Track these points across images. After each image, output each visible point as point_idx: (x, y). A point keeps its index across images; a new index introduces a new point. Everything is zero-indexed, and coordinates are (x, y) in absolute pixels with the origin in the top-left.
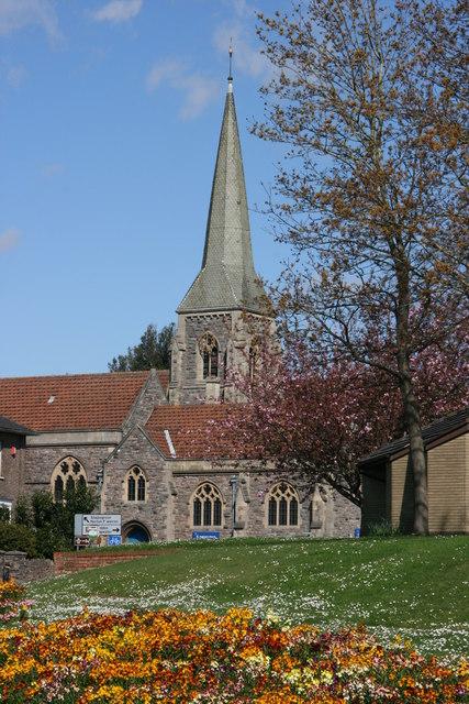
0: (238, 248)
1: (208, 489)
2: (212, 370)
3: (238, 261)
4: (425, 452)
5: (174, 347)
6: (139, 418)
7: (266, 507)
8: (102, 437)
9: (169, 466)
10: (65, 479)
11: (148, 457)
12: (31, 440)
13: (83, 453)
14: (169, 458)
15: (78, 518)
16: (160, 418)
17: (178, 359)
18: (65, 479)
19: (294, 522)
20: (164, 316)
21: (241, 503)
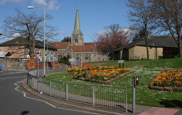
0: (79, 27)
1: (87, 55)
2: (76, 42)
3: (79, 29)
4: (39, 45)
5: (71, 39)
6: (68, 47)
7: (84, 58)
8: (64, 50)
9: (72, 53)
10: (59, 55)
11: (70, 52)
12: (57, 50)
13: (62, 52)
14: (72, 52)
15: (69, 59)
16: (70, 47)
17: (72, 40)
18: (59, 55)
19: (88, 59)
20: (69, 35)
21: (81, 57)
